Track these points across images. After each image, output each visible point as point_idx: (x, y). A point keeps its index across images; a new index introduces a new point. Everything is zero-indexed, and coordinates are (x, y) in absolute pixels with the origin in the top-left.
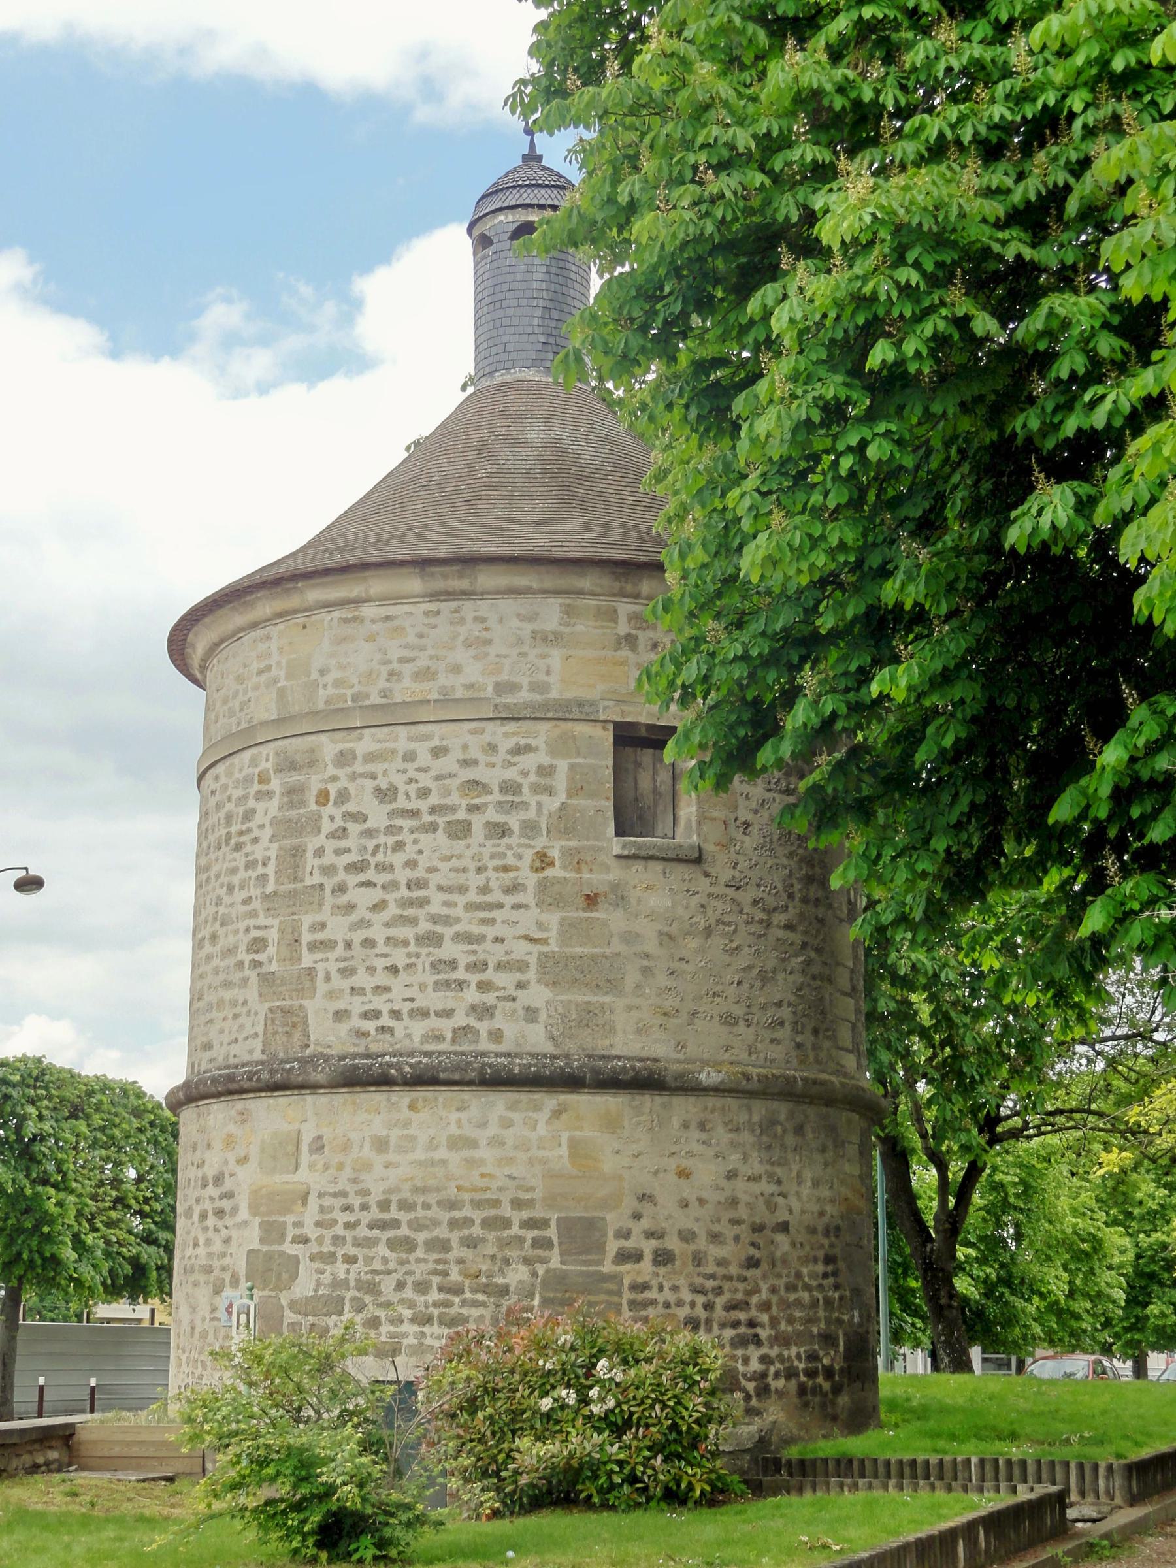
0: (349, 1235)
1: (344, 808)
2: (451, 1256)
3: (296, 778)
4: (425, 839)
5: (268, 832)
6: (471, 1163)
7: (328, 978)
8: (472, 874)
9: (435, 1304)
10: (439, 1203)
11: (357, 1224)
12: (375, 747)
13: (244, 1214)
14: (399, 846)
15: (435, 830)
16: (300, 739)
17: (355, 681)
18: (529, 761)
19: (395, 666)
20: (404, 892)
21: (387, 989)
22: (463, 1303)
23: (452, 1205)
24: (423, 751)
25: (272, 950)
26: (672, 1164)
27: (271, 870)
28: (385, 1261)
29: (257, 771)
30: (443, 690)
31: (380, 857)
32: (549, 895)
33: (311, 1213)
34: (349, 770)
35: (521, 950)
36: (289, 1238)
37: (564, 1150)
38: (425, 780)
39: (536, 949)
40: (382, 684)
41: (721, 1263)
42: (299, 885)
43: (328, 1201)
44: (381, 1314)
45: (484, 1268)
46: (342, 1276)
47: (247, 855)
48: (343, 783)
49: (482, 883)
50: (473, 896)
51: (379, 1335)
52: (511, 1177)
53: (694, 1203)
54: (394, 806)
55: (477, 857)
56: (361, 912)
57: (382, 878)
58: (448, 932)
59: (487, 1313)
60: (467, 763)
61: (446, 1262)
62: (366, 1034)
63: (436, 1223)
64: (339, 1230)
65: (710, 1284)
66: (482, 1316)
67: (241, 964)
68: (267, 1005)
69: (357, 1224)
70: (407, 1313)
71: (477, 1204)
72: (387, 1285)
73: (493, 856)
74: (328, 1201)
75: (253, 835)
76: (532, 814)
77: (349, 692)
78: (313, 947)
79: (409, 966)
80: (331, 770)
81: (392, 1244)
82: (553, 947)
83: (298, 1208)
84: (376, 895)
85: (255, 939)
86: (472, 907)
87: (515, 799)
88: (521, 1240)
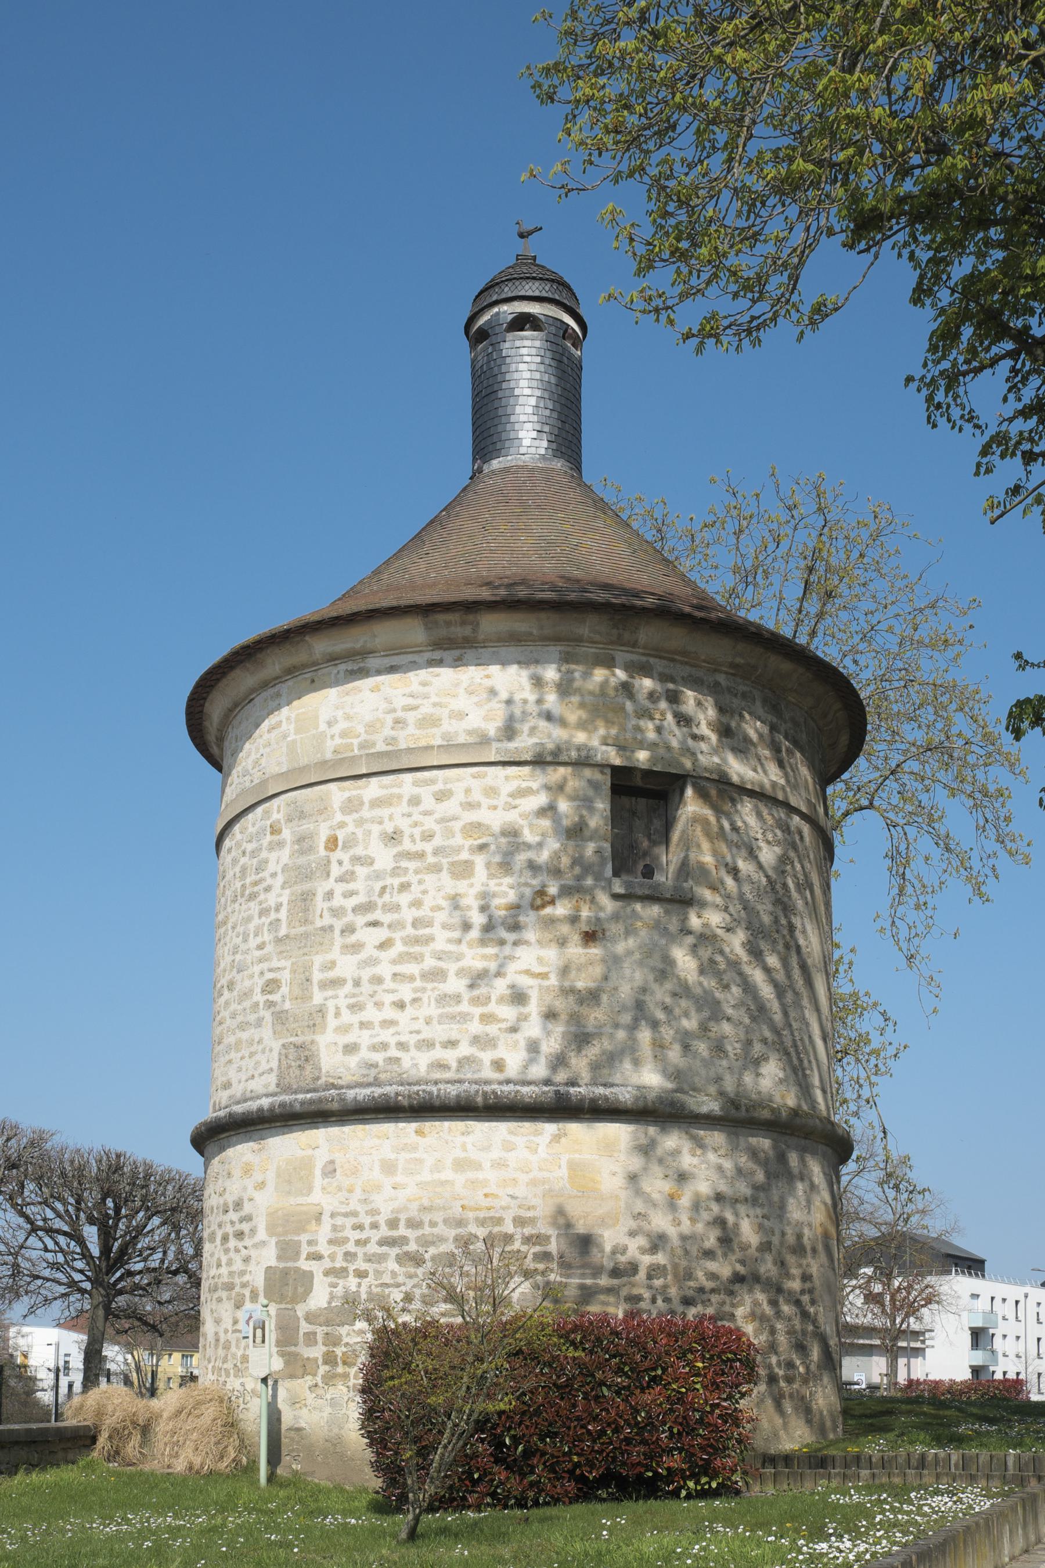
0: (360, 1251)
1: (352, 852)
3: (307, 826)
4: (430, 879)
5: (280, 879)
7: (337, 1014)
11: (366, 1242)
13: (262, 1235)
14: (404, 887)
15: (440, 870)
17: (362, 731)
19: (400, 714)
20: (410, 930)
21: (392, 1023)
23: (460, 1223)
24: (426, 794)
25: (285, 990)
27: (283, 914)
28: (394, 1274)
33: (324, 1232)
34: (355, 816)
36: (304, 1256)
37: (564, 1172)
38: (429, 823)
40: (387, 732)
42: (310, 928)
43: (339, 1221)
47: (261, 903)
48: (351, 828)
52: (512, 1197)
56: (369, 951)
57: (386, 918)
60: (470, 806)
62: (375, 1066)
64: (351, 1247)
69: (366, 1242)
71: (482, 1222)
74: (339, 1221)
77: (355, 742)
78: (324, 985)
79: (415, 1000)
80: (339, 817)
83: (313, 1226)
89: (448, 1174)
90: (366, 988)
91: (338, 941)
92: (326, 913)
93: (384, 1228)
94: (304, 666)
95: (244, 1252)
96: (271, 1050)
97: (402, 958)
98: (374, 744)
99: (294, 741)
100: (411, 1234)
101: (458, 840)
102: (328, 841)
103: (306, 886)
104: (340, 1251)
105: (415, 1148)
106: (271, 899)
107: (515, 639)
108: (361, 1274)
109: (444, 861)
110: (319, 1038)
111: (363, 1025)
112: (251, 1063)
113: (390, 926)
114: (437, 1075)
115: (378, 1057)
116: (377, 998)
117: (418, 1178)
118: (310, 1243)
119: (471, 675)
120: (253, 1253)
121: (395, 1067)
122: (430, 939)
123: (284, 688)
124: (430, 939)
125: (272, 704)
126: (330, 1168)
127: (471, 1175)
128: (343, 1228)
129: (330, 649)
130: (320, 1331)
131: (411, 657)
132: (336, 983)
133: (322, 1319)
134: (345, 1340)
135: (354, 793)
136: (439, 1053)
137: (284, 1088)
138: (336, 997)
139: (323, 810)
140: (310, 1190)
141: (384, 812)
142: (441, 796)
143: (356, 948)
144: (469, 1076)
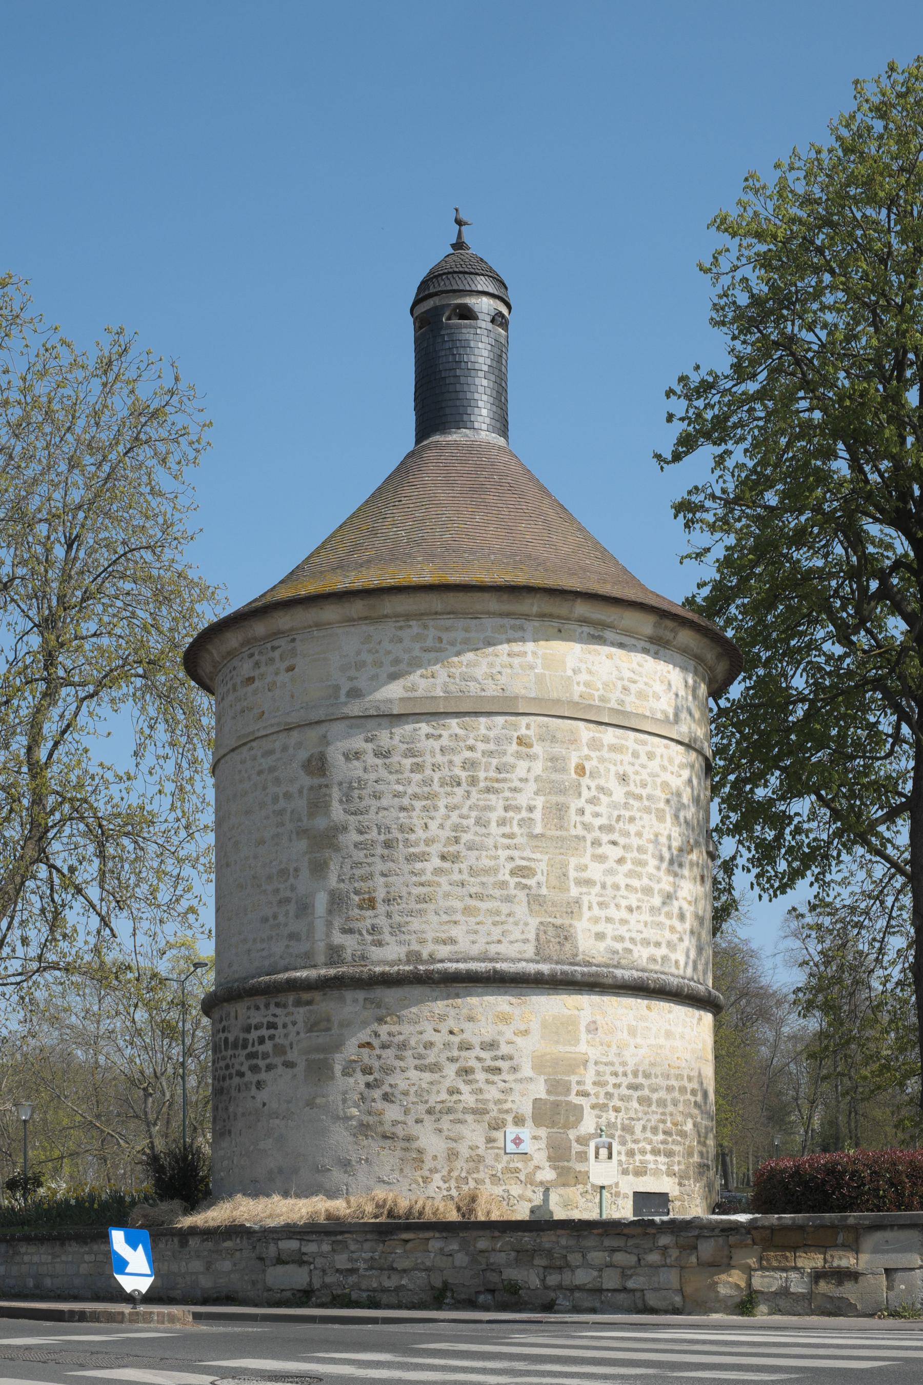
0: (616, 1092)
3: (557, 749)
5: (532, 787)
7: (590, 908)
12: (614, 741)
14: (632, 819)
16: (560, 720)
19: (626, 683)
25: (539, 877)
27: (537, 815)
29: (516, 734)
33: (589, 1076)
36: (574, 1092)
38: (645, 776)
42: (564, 833)
43: (601, 1068)
44: (635, 1146)
56: (611, 863)
64: (610, 1089)
67: (503, 885)
70: (649, 1147)
74: (601, 1068)
75: (513, 785)
77: (596, 694)
79: (638, 907)
80: (586, 751)
85: (521, 868)
90: (609, 891)
91: (589, 851)
92: (578, 825)
93: (630, 1076)
94: (559, 617)
96: (526, 924)
97: (630, 874)
99: (543, 675)
102: (577, 767)
103: (561, 799)
104: (602, 1091)
106: (522, 800)
111: (609, 920)
112: (496, 932)
115: (619, 946)
116: (616, 901)
118: (578, 1083)
123: (529, 626)
125: (511, 634)
126: (592, 1027)
129: (587, 615)
131: (633, 641)
135: (597, 735)
137: (540, 956)
138: (589, 893)
140: (577, 1041)
143: (602, 858)
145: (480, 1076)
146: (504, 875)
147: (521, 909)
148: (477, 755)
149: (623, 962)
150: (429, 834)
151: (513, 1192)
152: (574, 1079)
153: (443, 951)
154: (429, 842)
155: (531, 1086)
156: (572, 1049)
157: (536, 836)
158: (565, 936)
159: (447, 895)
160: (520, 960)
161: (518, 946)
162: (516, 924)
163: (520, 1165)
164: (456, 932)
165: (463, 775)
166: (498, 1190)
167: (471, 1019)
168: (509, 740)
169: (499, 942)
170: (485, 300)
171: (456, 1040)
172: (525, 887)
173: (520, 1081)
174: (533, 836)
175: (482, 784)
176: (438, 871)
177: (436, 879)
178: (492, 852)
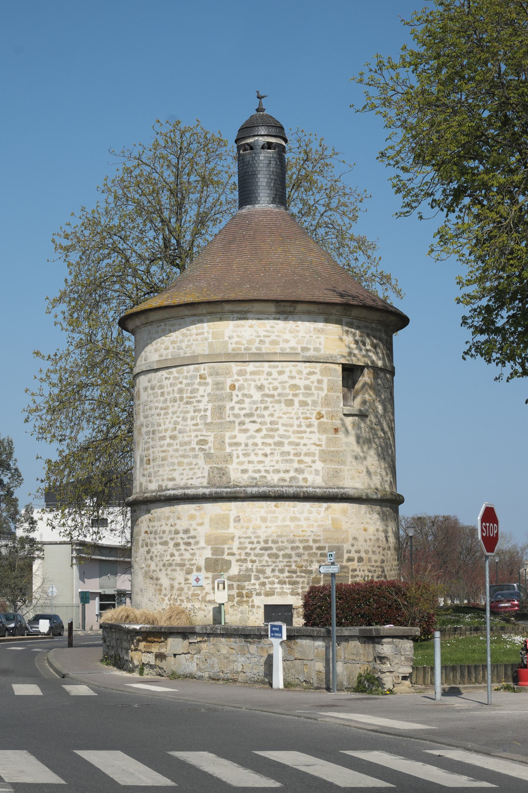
0: (252, 552)
1: (242, 392)
2: (292, 560)
3: (220, 379)
4: (277, 406)
5: (206, 399)
6: (298, 526)
7: (238, 457)
8: (295, 420)
9: (287, 577)
10: (287, 541)
11: (255, 549)
12: (255, 369)
13: (202, 544)
14: (266, 408)
15: (281, 403)
17: (245, 343)
18: (314, 378)
19: (262, 338)
20: (269, 426)
21: (262, 462)
22: (297, 577)
23: (293, 542)
24: (274, 371)
25: (210, 445)
26: (362, 526)
27: (209, 413)
28: (267, 561)
29: (198, 374)
30: (281, 349)
31: (258, 412)
32: (322, 429)
33: (235, 545)
34: (244, 377)
35: (313, 448)
36: (226, 553)
37: (330, 522)
38: (276, 383)
39: (319, 448)
40: (257, 345)
41: (376, 561)
42: (223, 421)
44: (266, 581)
45: (304, 564)
46: (250, 567)
47: (195, 407)
48: (241, 382)
49: (299, 423)
50: (295, 428)
51: (266, 588)
52: (312, 532)
53: (368, 540)
54: (263, 392)
55: (297, 413)
56: (251, 433)
57: (259, 420)
58: (286, 441)
59: (306, 580)
60: (292, 377)
61: (290, 562)
62: (256, 479)
63: (286, 548)
64: (248, 551)
65: (373, 569)
66: (304, 581)
67: (193, 449)
68: (209, 466)
69: (255, 549)
70: (276, 581)
71: (301, 541)
72: (268, 571)
73: (302, 413)
74: (242, 540)
75: (197, 399)
76: (315, 398)
77: (243, 347)
78: (231, 445)
79: (272, 453)
80: (236, 377)
81: (269, 556)
82: (324, 447)
83: (230, 542)
84: (257, 426)
85: (201, 441)
86: (294, 432)
87: (310, 392)
88: (316, 554)
89: (288, 523)
90: (250, 447)
91: (237, 427)
92: (231, 415)
94: (218, 313)
95: (191, 551)
96: (204, 469)
98: (251, 349)
99: (212, 342)
100: (273, 545)
101: (287, 391)
102: (231, 386)
103: (221, 403)
104: (243, 552)
105: (274, 512)
106: (201, 406)
107: (309, 313)
108: (253, 562)
109: (282, 399)
110: (229, 466)
111: (249, 462)
112: (191, 473)
113: (260, 423)
114: (282, 484)
115: (257, 475)
117: (276, 524)
118: (229, 549)
119: (291, 324)
120: (197, 552)
121: (264, 480)
122: (277, 430)
124: (277, 430)
126: (238, 519)
127: (297, 523)
128: (244, 543)
130: (235, 584)
132: (237, 444)
133: (236, 579)
134: (247, 587)
136: (282, 475)
137: (211, 484)
138: (237, 450)
139: (228, 373)
140: (228, 527)
141: (257, 377)
142: (281, 373)
143: (246, 431)
144: (294, 484)
145: (182, 547)
146: (194, 445)
147: (201, 461)
148: (183, 386)
149: (259, 483)
150: (166, 427)
151: (196, 606)
152: (226, 547)
153: (170, 484)
154: (166, 430)
155: (204, 552)
156: (225, 531)
157: (208, 424)
158: (223, 472)
159: (172, 456)
160: (200, 487)
161: (200, 480)
162: (199, 469)
163: (199, 592)
164: (175, 475)
165: (178, 396)
166: (189, 605)
167: (179, 518)
168: (195, 377)
169: (192, 478)
170: (263, 133)
171: (173, 529)
172: (203, 450)
173: (199, 549)
174: (206, 424)
175: (185, 400)
176: (169, 445)
177: (168, 448)
178: (189, 434)
